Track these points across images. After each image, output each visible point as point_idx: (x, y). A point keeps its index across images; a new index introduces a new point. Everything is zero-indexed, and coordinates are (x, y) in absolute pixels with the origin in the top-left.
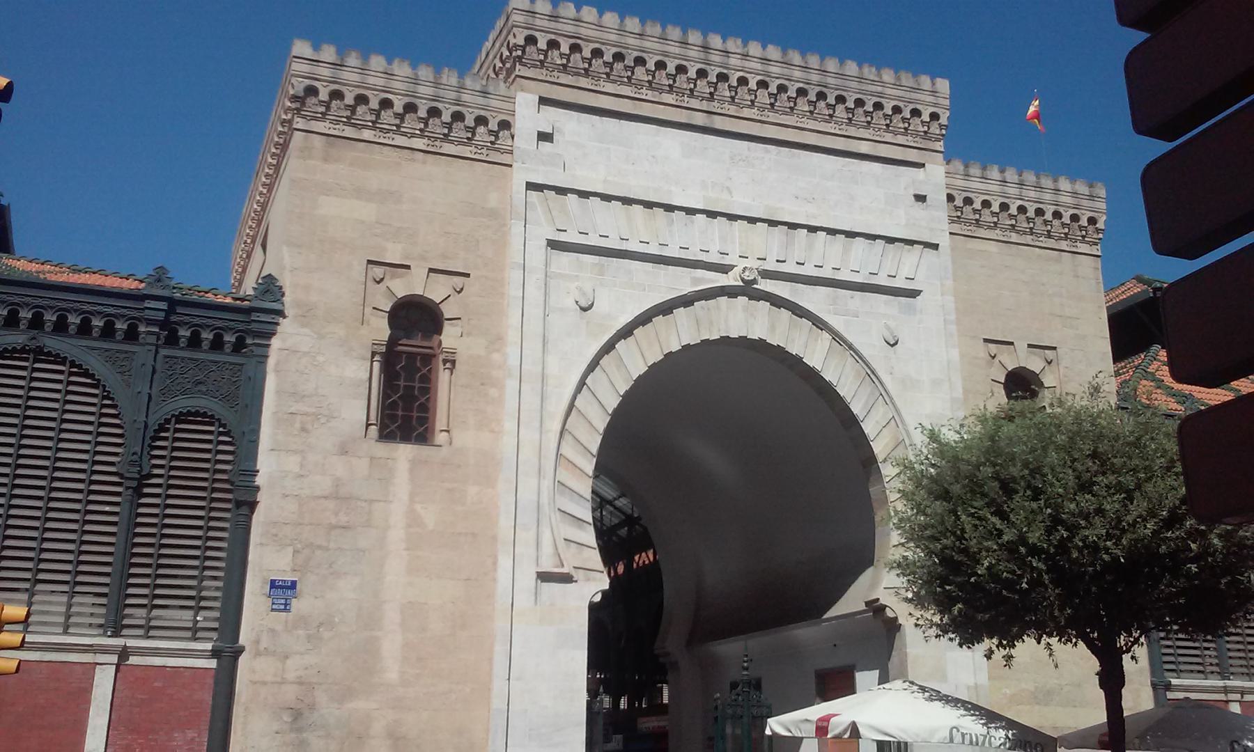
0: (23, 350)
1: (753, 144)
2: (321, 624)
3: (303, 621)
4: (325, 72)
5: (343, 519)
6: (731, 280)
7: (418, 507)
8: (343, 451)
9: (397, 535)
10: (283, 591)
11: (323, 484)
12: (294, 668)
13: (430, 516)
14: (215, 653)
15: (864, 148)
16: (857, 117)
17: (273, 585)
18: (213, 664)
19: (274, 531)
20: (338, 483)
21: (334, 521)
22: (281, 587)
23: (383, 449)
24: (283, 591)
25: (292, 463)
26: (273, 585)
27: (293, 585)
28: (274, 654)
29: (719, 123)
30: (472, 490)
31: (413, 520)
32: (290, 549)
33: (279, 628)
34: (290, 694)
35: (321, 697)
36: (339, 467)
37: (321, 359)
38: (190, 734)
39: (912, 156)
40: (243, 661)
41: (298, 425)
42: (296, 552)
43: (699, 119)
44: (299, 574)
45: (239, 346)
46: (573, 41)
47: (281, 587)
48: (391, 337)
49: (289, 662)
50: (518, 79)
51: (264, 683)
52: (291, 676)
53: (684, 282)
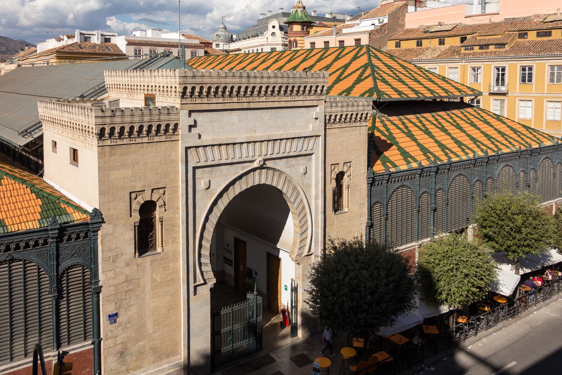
0: (5, 261)
1: (263, 110)
2: (126, 323)
3: (121, 324)
4: (108, 120)
5: (130, 287)
6: (256, 165)
7: (154, 276)
8: (128, 265)
9: (148, 287)
10: (113, 317)
11: (122, 278)
12: (119, 340)
13: (158, 279)
14: (93, 343)
15: (300, 104)
16: (230, 252)
17: (110, 316)
18: (92, 346)
19: (108, 299)
20: (127, 276)
21: (127, 289)
22: (112, 316)
23: (140, 260)
24: (113, 317)
25: (111, 274)
26: (110, 316)
27: (116, 314)
28: (112, 338)
29: (252, 105)
30: (172, 265)
31: (153, 280)
32: (114, 303)
33: (113, 329)
34: (119, 348)
35: (129, 345)
36: (127, 271)
37: (117, 234)
38: (88, 370)
39: (315, 103)
40: (102, 342)
41: (111, 260)
42: (116, 303)
43: (245, 106)
44: (117, 310)
45: (86, 236)
46: (200, 85)
47: (112, 316)
48: (140, 219)
49: (117, 338)
50: (188, 150)
51: (110, 347)
52: (118, 342)
53: (240, 170)
